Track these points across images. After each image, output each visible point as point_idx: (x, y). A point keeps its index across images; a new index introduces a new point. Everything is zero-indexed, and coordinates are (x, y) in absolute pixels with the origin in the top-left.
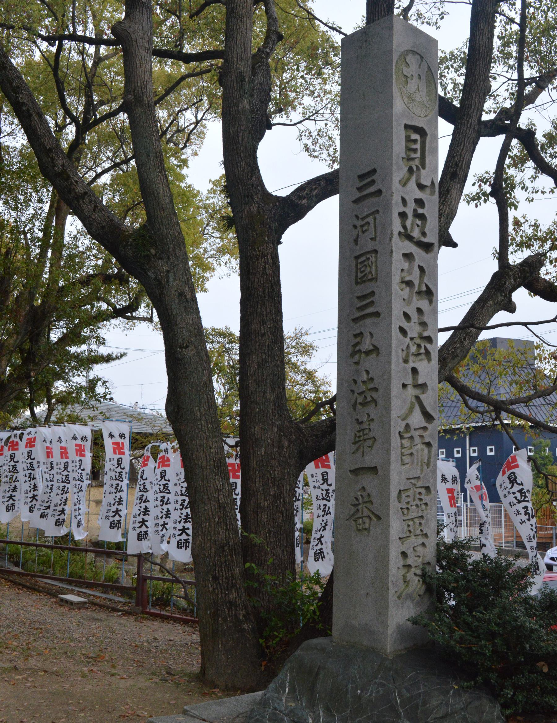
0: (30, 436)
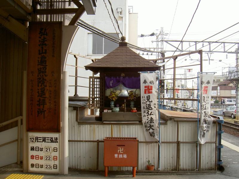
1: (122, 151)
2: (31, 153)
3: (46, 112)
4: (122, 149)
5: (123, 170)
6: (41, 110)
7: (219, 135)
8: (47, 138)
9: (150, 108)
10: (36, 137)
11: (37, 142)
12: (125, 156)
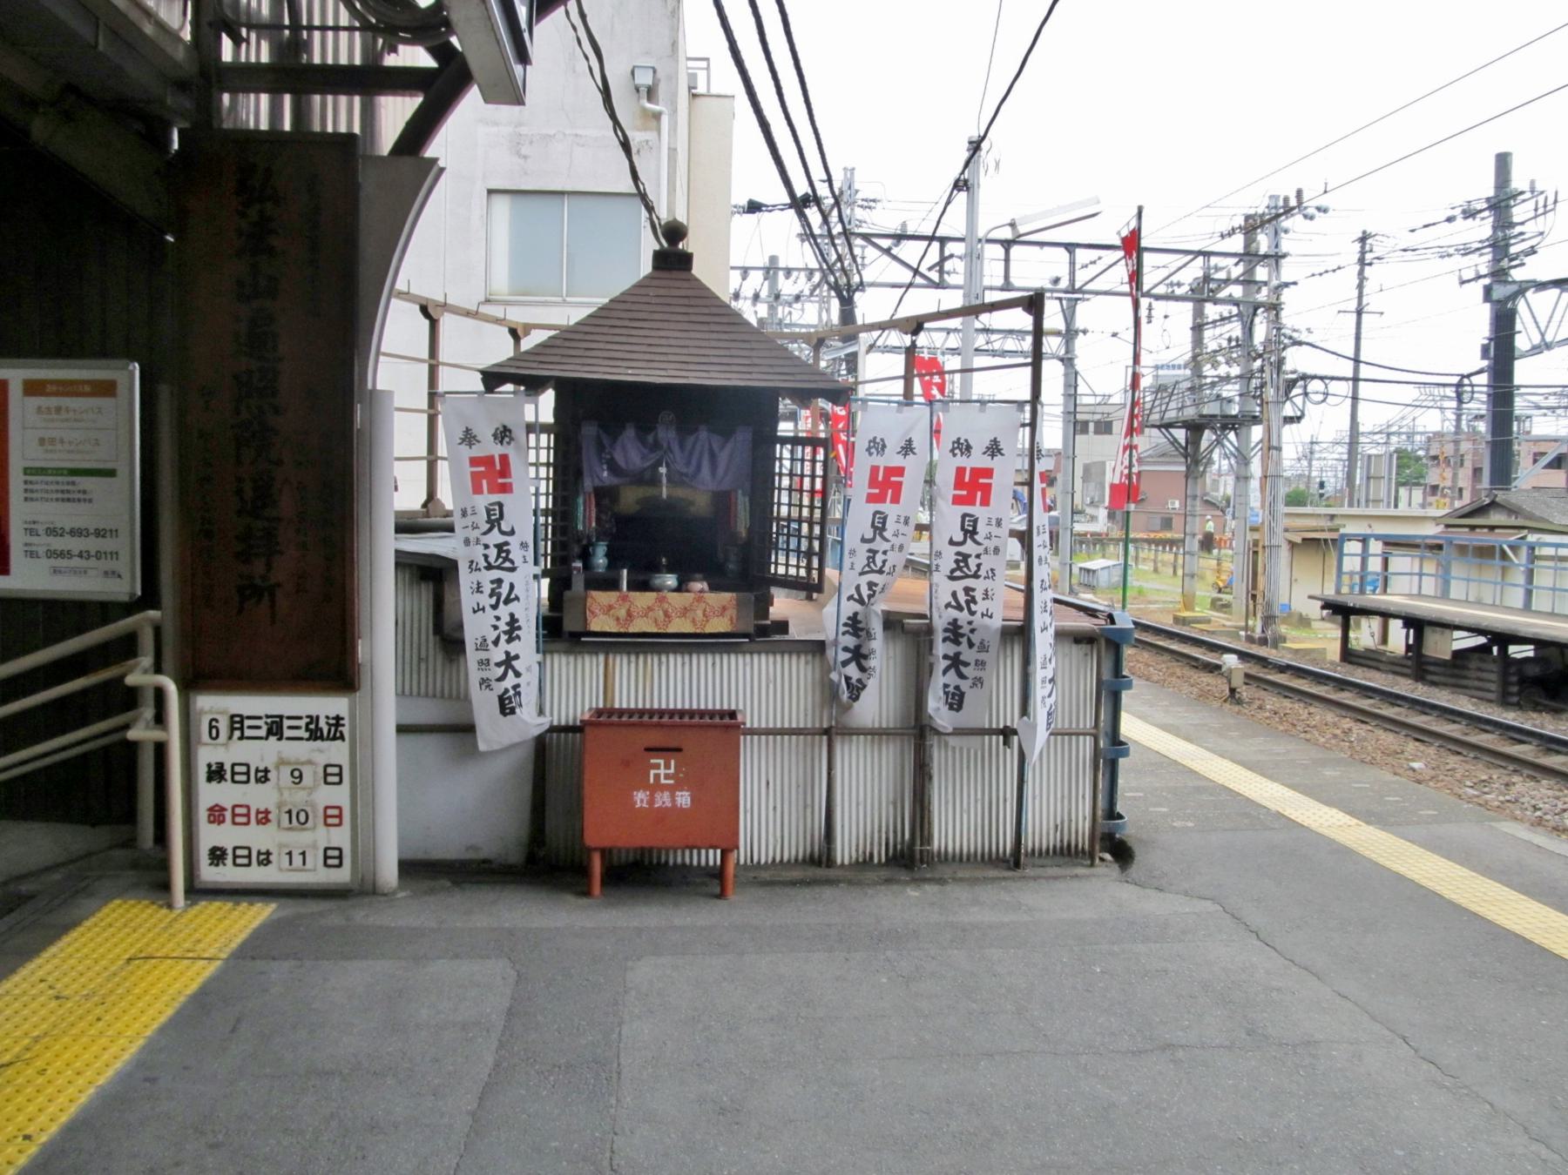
0: (882, 462)
1: (667, 777)
2: (210, 794)
3: (279, 594)
4: (667, 766)
5: (687, 861)
6: (258, 581)
7: (1111, 694)
8: (289, 718)
9: (507, 564)
10: (232, 717)
11: (242, 738)
12: (684, 799)
